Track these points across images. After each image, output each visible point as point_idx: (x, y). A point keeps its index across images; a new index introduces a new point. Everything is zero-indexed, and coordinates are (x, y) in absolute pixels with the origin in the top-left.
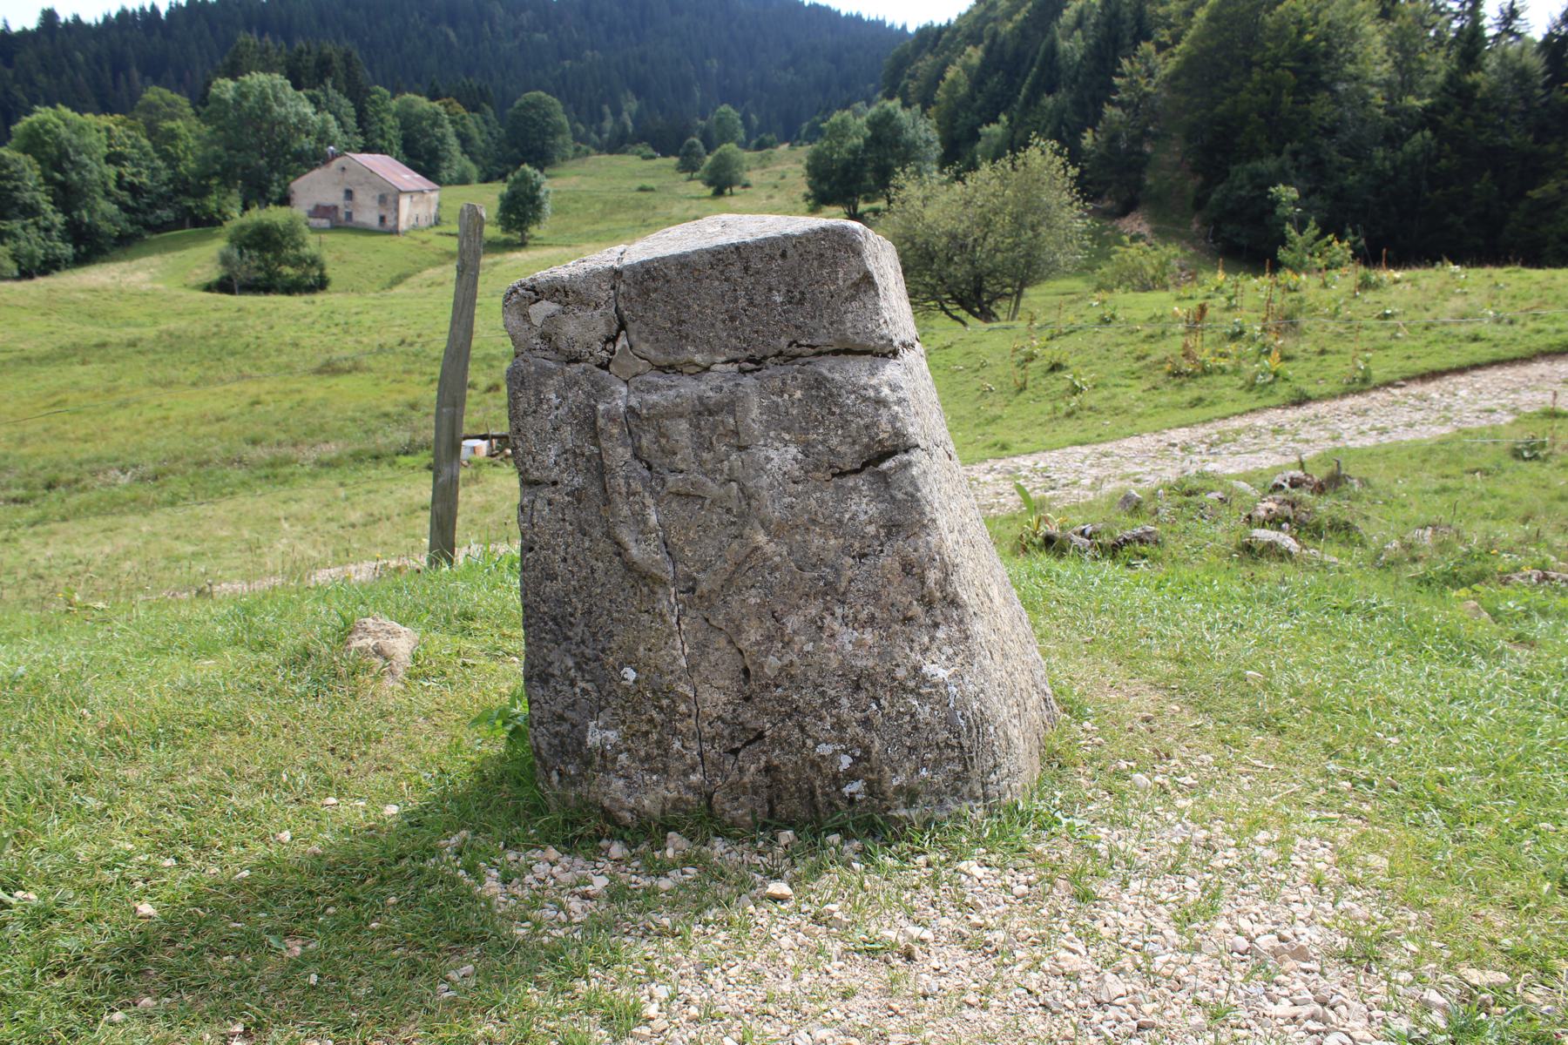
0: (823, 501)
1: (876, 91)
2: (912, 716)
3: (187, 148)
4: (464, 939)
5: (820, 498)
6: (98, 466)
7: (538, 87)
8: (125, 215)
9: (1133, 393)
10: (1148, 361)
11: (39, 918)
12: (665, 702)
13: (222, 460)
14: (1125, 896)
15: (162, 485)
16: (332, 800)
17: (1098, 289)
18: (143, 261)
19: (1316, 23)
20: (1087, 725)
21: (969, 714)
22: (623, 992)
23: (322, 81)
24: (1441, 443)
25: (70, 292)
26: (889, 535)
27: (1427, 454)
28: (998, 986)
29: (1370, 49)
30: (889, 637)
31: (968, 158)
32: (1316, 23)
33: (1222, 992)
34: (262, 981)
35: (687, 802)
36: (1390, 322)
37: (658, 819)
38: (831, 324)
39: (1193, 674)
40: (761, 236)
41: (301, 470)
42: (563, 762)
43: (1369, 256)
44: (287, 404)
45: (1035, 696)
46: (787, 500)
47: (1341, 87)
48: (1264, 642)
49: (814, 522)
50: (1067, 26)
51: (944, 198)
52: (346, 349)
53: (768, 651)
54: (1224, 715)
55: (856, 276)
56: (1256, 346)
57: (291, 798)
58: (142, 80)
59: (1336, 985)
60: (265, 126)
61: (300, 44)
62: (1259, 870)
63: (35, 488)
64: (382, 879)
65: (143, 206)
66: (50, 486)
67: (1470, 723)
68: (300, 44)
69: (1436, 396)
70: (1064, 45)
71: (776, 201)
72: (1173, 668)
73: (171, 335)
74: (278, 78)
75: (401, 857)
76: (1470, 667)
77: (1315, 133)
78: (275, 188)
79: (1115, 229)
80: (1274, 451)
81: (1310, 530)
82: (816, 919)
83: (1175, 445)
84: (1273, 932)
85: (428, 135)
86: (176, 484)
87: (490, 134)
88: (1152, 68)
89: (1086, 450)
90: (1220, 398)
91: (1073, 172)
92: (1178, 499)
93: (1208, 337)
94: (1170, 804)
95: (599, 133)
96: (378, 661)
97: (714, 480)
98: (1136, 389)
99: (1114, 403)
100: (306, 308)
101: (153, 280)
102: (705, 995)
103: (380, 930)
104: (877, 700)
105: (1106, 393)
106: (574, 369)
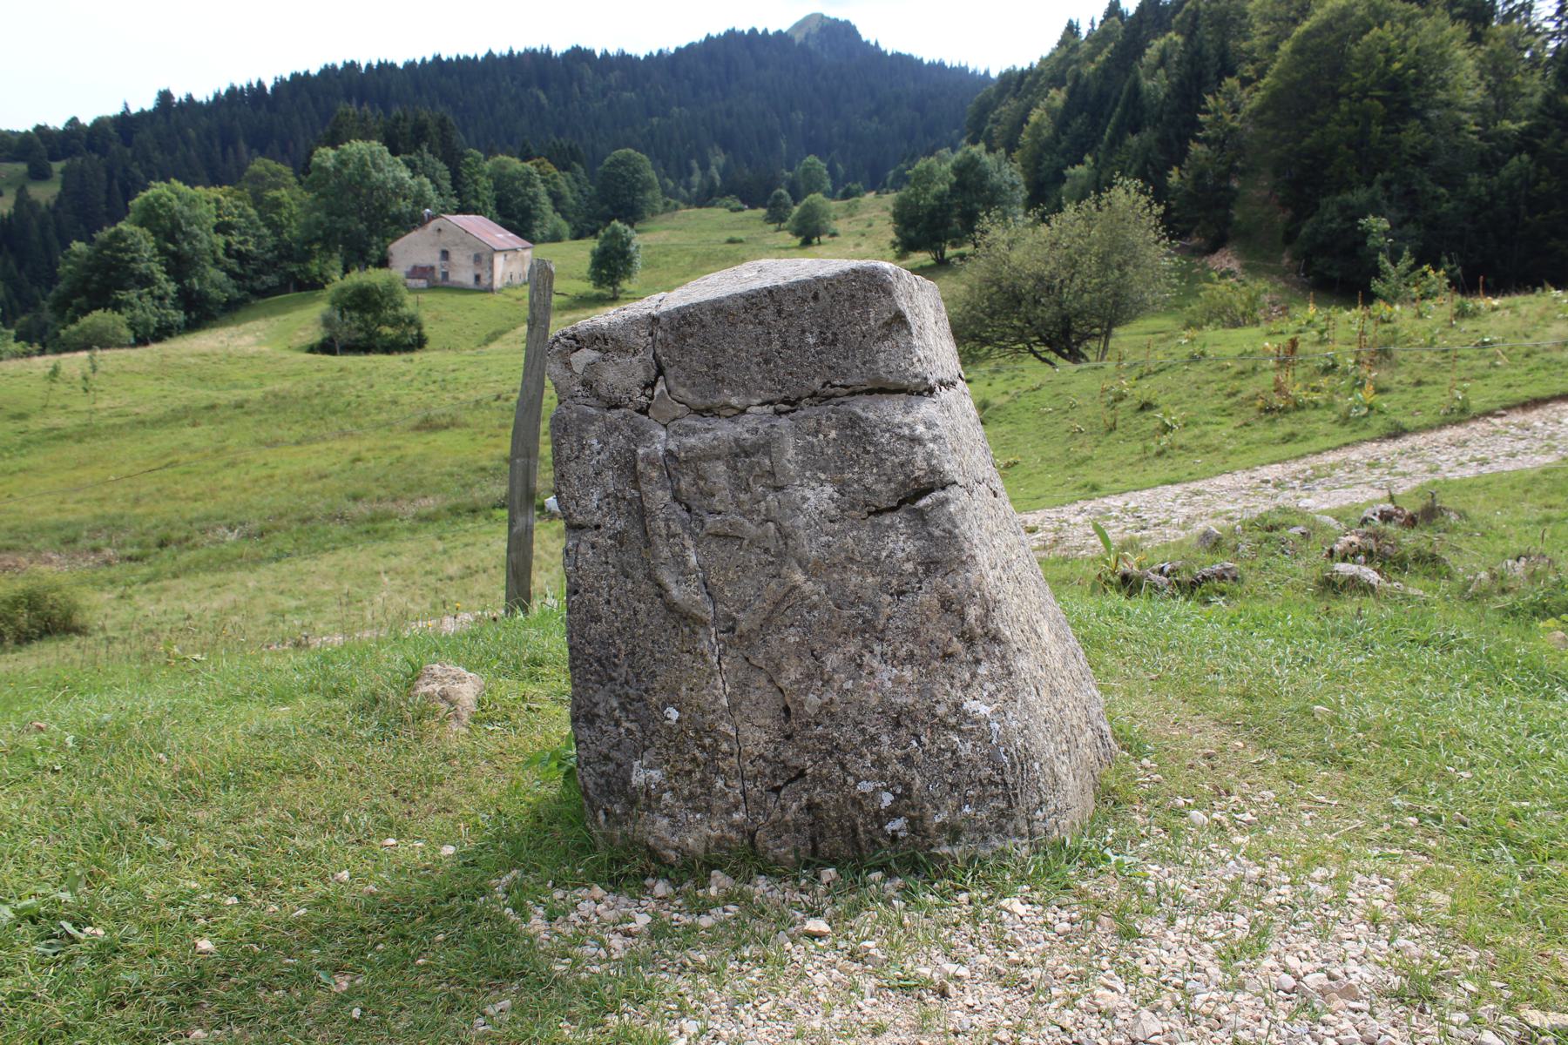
0: (860, 540)
1: (961, 137)
2: (954, 753)
3: (291, 215)
4: (503, 975)
5: (855, 538)
6: (207, 524)
7: (628, 144)
8: (232, 281)
9: (1224, 431)
10: (1239, 397)
11: (105, 953)
12: (707, 741)
13: (325, 516)
14: (1170, 934)
15: (268, 542)
16: (391, 841)
17: (1187, 327)
18: (250, 325)
19: (1404, 51)
20: (1145, 762)
21: (1012, 750)
22: (654, 1026)
23: (418, 146)
24: (1545, 472)
25: (180, 357)
26: (927, 572)
27: (1529, 484)
28: (1030, 1023)
29: (1462, 75)
30: (929, 674)
31: (1054, 200)
32: (1404, 51)
33: (1264, 1031)
34: (308, 1015)
35: (731, 840)
36: (1489, 350)
37: (702, 857)
38: (864, 364)
39: (1259, 710)
40: (794, 279)
41: (400, 525)
42: (609, 801)
43: (1465, 285)
44: (386, 461)
45: (1089, 734)
46: (824, 539)
47: (1432, 114)
48: (1336, 676)
49: (851, 560)
50: (1150, 65)
51: (1029, 240)
52: (443, 404)
53: (808, 689)
54: (1289, 752)
55: (887, 316)
56: (1349, 380)
57: (352, 839)
58: (249, 153)
59: (1385, 1025)
60: (364, 191)
61: (396, 111)
62: (1312, 908)
63: (148, 546)
64: (432, 916)
65: (250, 273)
66: (162, 544)
67: (1549, 756)
68: (396, 111)
69: (1539, 424)
70: (1147, 84)
71: (864, 248)
72: (1239, 704)
73: (276, 396)
74: (376, 145)
75: (453, 896)
76: (1552, 699)
77: (1406, 162)
78: (374, 251)
79: (1204, 266)
80: (1371, 485)
81: (1390, 561)
82: (852, 956)
83: (1267, 482)
84: (1321, 970)
85: (520, 195)
86: (282, 541)
87: (581, 191)
88: (1238, 103)
89: (1177, 489)
90: (1314, 433)
91: (1159, 210)
92: (1259, 535)
93: (1300, 372)
94: (1225, 841)
95: (688, 187)
96: (444, 706)
97: (751, 521)
98: (1228, 427)
99: (1206, 441)
100: (404, 367)
101: (260, 342)
102: (735, 1031)
103: (425, 966)
104: (917, 737)
105: (1196, 431)
106: (614, 415)
